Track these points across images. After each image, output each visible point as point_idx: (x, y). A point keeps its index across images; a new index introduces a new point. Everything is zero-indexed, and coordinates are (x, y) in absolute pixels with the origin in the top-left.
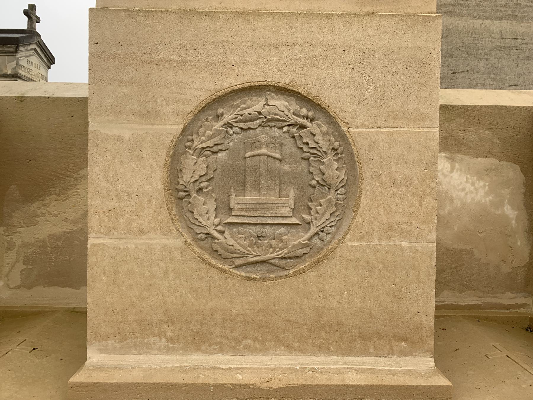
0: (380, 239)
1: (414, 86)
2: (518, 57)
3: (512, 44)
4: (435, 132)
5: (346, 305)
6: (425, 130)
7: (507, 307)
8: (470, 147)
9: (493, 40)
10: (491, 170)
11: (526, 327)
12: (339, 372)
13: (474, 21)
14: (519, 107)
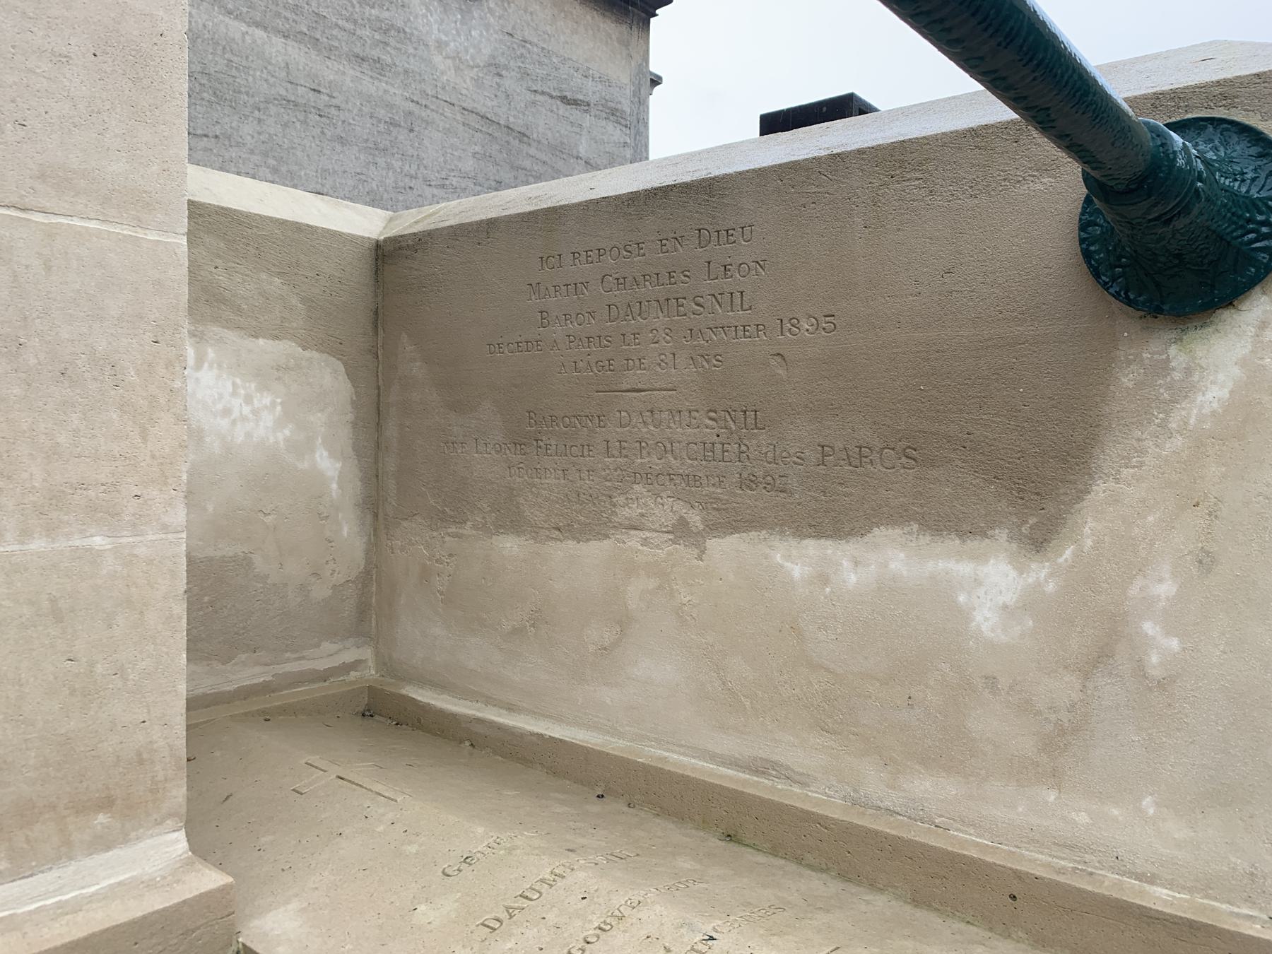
0: (25, 534)
1: (118, 110)
2: (323, 133)
3: (309, 100)
4: (179, 245)
6: (152, 236)
7: (324, 676)
8: (239, 311)
9: (272, 80)
10: (287, 369)
11: (361, 709)
13: (227, 20)
14: (340, 234)
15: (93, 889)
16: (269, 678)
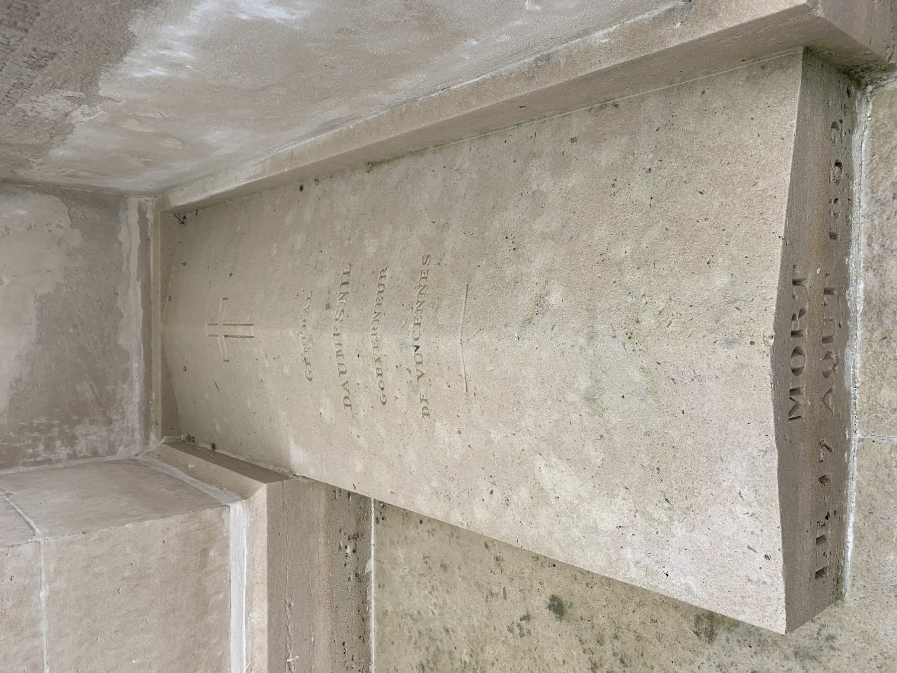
0: (36, 635)
5: (154, 655)
12: (251, 636)
15: (246, 551)
16: (139, 284)
